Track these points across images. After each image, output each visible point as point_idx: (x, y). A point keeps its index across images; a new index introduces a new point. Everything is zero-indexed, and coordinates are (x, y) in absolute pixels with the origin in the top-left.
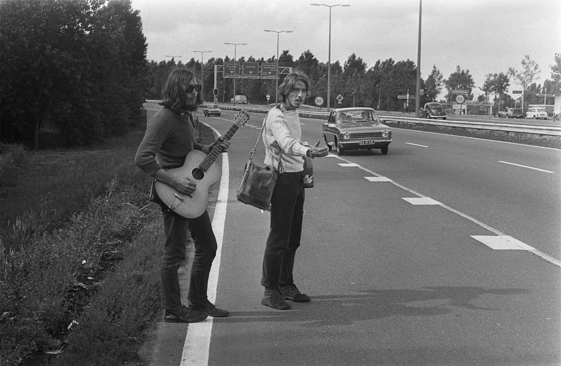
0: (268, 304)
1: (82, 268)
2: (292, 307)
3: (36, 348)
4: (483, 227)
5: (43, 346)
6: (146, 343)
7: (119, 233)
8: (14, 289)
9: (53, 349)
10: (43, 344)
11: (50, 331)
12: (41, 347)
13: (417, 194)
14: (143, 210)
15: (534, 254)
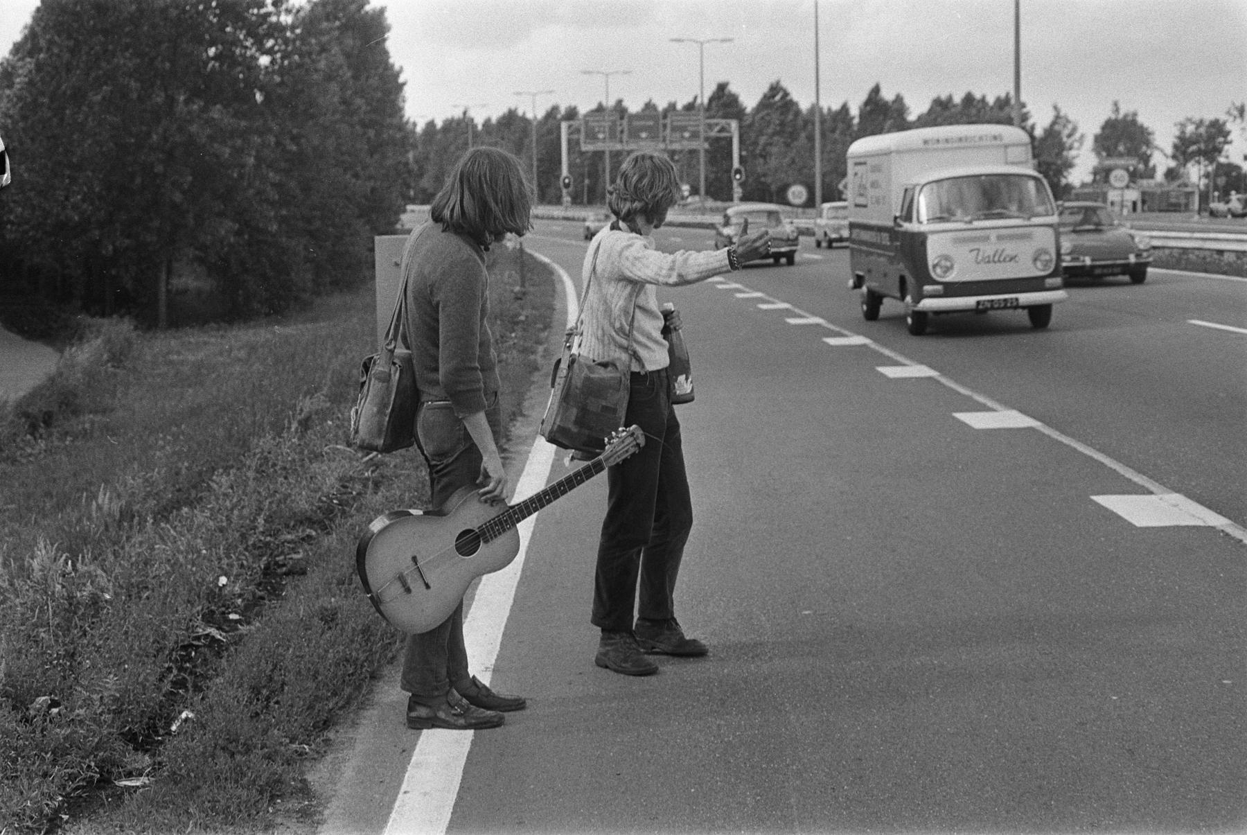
0: (609, 665)
1: (215, 594)
2: (661, 668)
3: (96, 772)
4: (1123, 476)
5: (113, 770)
6: (329, 758)
7: (309, 514)
8: (66, 645)
9: (133, 776)
10: (113, 765)
11: (130, 738)
12: (109, 772)
13: (990, 403)
14: (371, 459)
15: (1227, 535)
